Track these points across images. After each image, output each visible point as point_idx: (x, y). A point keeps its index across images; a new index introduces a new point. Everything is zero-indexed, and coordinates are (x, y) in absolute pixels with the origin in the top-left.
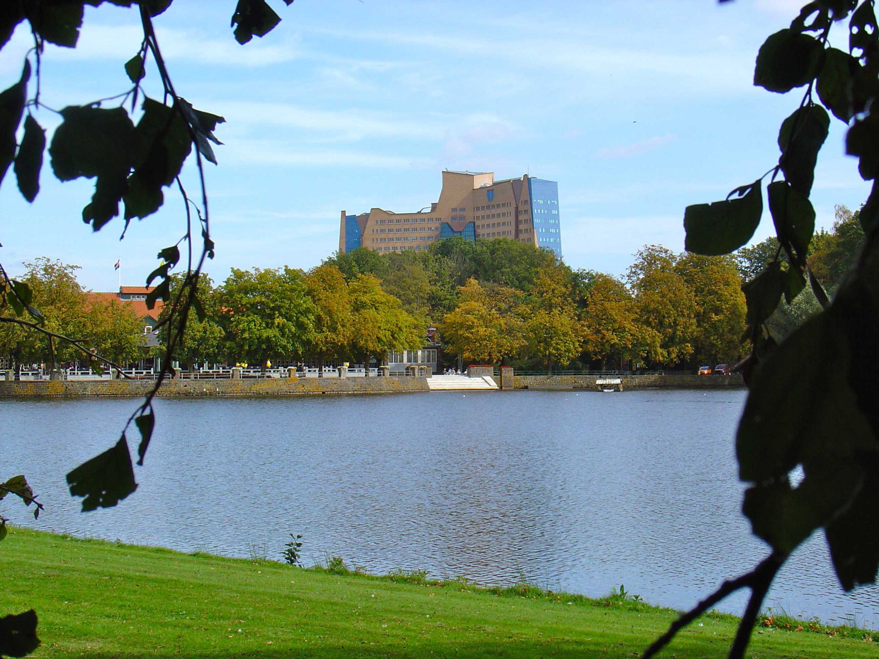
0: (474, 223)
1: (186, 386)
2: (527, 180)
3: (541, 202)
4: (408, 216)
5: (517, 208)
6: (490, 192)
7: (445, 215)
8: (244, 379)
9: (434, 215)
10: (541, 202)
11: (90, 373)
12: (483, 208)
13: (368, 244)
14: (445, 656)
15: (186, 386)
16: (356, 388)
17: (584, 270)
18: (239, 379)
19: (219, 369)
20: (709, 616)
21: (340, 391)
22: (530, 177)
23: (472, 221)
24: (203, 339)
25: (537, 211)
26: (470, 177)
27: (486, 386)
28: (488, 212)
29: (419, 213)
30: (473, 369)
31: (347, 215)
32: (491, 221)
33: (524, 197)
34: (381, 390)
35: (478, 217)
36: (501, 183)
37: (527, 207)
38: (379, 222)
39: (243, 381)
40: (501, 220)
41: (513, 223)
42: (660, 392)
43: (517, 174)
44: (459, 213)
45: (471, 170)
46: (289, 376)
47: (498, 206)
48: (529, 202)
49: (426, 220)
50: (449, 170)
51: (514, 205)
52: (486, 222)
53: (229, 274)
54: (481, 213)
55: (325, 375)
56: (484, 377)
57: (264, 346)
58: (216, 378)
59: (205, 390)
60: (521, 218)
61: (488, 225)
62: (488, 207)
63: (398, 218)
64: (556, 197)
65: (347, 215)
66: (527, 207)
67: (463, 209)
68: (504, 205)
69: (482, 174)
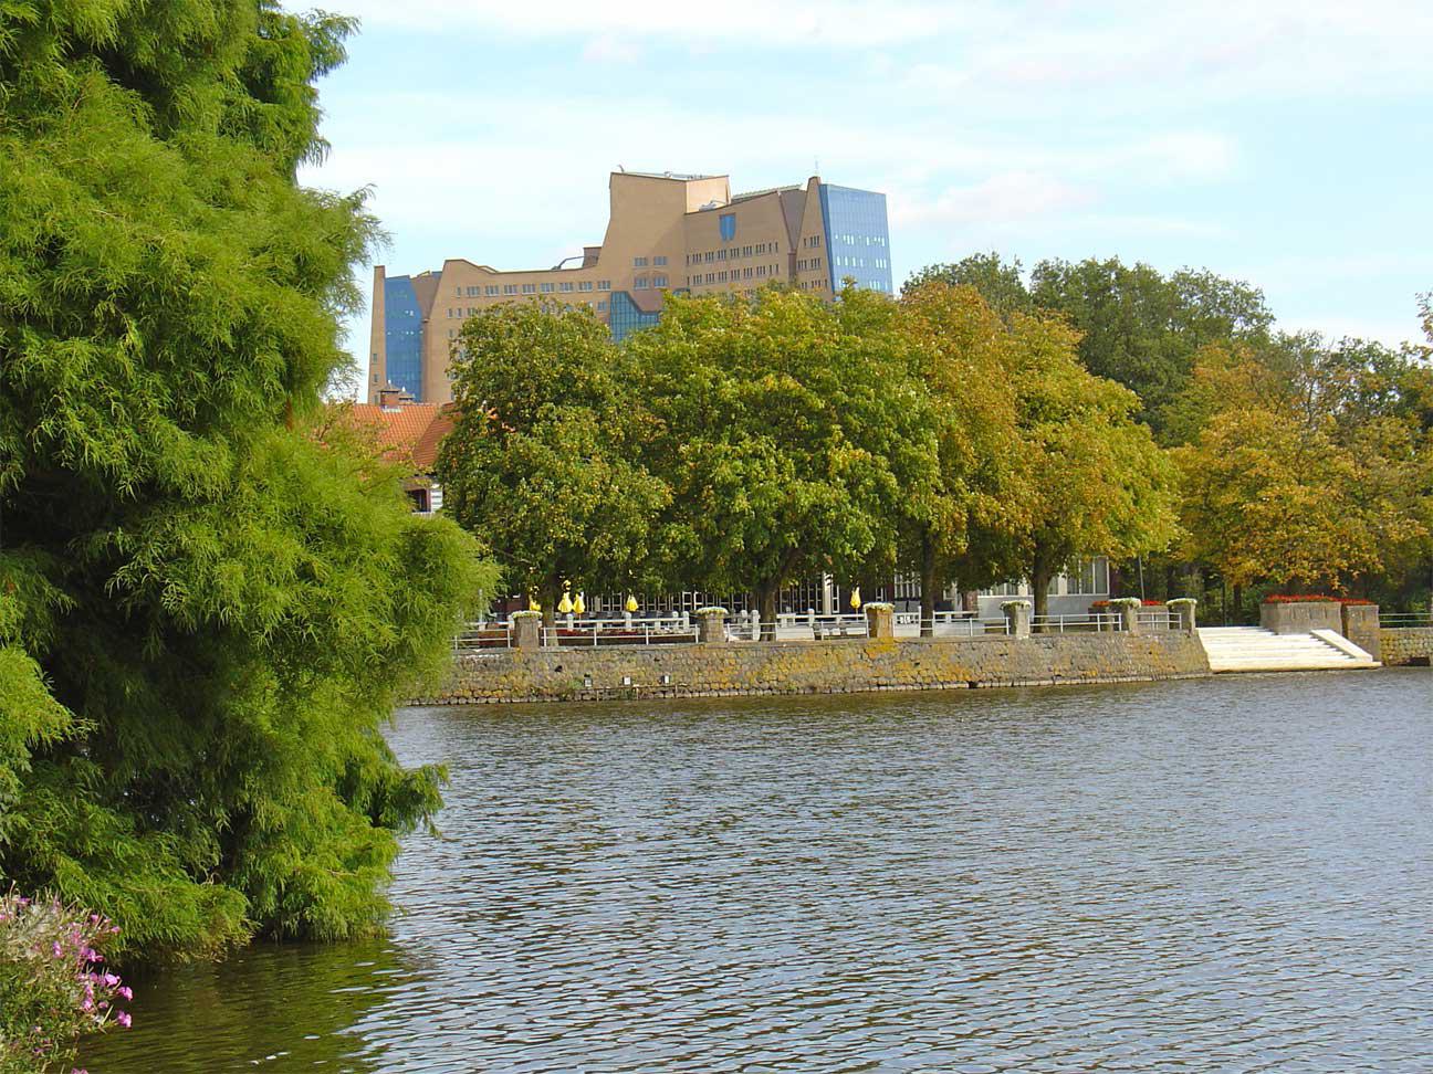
1: (559, 669)
3: (851, 240)
4: (532, 275)
5: (793, 255)
6: (728, 219)
7: (621, 275)
8: (654, 646)
9: (593, 274)
10: (851, 240)
12: (709, 256)
15: (559, 669)
16: (1058, 668)
17: (1359, 342)
21: (1020, 678)
22: (823, 182)
24: (601, 518)
25: (842, 261)
26: (677, 185)
28: (721, 266)
29: (557, 269)
30: (1285, 609)
31: (387, 276)
33: (811, 227)
34: (1122, 673)
35: (697, 279)
36: (752, 198)
37: (819, 253)
38: (464, 292)
42: (1404, 681)
44: (652, 269)
45: (678, 169)
46: (873, 634)
47: (747, 251)
49: (576, 286)
50: (627, 171)
51: (785, 249)
54: (704, 269)
56: (1318, 632)
57: (792, 539)
59: (627, 681)
62: (722, 254)
63: (510, 281)
64: (883, 228)
65: (387, 276)
66: (819, 253)
67: (661, 261)
68: (760, 249)
69: (701, 178)
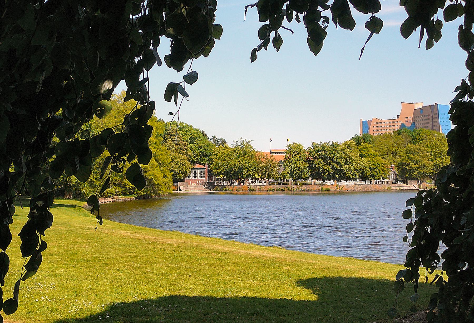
0: (415, 123)
2: (437, 105)
11: (350, 182)
13: (371, 133)
14: (356, 282)
18: (314, 185)
19: (223, 182)
20: (15, 215)
23: (414, 122)
27: (414, 188)
32: (422, 122)
39: (316, 186)
40: (426, 122)
41: (431, 123)
43: (430, 102)
47: (425, 116)
48: (437, 114)
52: (419, 122)
53: (310, 145)
54: (418, 119)
55: (367, 183)
58: (282, 185)
60: (434, 120)
61: (421, 124)
63: (384, 121)
69: (418, 103)
